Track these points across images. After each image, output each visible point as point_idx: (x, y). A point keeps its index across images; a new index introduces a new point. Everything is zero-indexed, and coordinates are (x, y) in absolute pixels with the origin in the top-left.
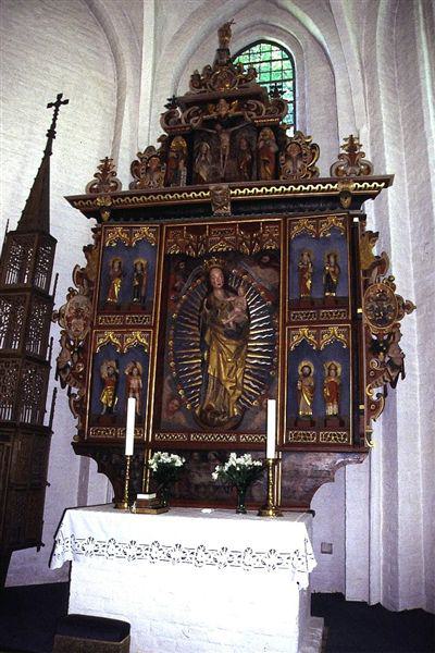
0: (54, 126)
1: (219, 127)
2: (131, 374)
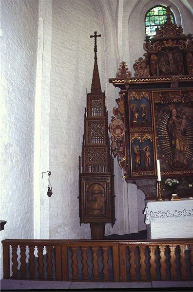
0: (96, 46)
1: (167, 51)
2: (146, 150)
